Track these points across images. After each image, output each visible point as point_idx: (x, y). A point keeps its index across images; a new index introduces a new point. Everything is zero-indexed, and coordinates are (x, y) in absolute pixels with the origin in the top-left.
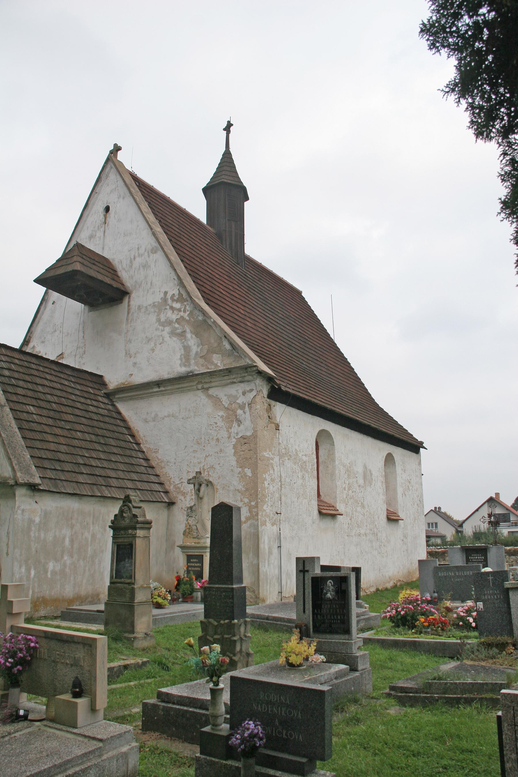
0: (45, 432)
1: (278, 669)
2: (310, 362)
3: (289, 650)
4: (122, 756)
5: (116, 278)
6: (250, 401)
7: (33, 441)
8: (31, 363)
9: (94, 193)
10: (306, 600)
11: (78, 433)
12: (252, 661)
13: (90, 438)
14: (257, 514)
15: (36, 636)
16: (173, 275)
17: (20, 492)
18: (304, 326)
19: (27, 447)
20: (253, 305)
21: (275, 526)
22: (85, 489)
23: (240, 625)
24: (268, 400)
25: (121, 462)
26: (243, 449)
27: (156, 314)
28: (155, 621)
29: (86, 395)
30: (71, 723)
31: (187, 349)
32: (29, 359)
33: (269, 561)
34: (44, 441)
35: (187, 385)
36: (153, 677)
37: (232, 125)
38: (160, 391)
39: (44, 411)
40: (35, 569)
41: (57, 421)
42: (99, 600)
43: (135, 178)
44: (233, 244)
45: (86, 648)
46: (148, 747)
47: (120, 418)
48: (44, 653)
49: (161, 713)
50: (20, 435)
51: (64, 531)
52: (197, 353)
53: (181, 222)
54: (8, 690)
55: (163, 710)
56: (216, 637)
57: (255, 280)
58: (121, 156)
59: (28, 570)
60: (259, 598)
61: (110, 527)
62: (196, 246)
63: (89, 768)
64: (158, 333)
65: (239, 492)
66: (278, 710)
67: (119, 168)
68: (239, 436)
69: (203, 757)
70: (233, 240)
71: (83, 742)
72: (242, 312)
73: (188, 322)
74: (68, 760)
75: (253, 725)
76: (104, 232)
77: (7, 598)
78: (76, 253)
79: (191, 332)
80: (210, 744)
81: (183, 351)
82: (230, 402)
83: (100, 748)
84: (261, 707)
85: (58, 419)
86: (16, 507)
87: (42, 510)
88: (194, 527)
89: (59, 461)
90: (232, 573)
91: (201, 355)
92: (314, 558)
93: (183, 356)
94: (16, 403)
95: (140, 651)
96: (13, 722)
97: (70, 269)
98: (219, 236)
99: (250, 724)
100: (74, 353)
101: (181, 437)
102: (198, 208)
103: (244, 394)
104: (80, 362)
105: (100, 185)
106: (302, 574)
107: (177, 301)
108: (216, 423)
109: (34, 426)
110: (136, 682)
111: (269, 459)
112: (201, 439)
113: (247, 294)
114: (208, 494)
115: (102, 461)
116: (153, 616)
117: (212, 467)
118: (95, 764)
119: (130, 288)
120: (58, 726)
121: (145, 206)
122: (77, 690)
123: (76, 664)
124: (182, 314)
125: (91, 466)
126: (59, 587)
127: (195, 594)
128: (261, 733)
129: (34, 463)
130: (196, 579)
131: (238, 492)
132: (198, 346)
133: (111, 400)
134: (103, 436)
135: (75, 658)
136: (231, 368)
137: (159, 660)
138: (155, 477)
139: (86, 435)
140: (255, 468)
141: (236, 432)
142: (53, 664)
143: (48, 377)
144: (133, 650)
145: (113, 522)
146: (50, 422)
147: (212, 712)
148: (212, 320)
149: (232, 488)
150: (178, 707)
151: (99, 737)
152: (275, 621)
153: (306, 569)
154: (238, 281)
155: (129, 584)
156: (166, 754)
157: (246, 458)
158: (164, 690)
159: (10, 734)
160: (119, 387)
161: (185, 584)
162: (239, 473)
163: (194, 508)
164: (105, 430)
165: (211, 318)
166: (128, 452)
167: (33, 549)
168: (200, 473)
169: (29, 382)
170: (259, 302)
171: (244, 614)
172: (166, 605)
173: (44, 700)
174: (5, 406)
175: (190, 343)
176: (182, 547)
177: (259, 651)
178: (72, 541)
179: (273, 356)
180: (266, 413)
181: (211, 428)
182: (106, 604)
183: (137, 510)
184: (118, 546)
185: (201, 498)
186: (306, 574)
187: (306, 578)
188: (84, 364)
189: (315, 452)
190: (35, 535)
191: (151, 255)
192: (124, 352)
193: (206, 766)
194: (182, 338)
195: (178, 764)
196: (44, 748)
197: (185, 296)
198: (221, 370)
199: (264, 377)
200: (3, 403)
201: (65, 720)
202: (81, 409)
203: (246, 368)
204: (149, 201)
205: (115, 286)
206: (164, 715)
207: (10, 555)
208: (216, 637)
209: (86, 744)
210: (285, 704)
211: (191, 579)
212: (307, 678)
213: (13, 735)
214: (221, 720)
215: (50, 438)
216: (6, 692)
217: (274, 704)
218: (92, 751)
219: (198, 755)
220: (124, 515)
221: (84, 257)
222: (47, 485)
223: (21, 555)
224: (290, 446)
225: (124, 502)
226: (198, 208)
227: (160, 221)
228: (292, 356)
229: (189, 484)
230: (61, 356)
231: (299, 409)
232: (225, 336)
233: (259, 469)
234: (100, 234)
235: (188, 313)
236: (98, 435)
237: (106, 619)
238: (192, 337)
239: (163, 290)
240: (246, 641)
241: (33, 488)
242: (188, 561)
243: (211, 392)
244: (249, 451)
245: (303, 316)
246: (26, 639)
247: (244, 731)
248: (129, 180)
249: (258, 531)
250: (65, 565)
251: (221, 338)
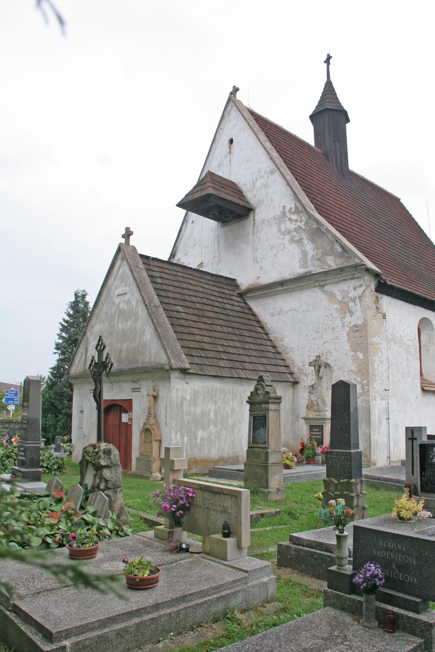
0: (192, 327)
1: (390, 521)
2: (411, 260)
3: (400, 506)
4: (263, 585)
5: (242, 198)
6: (360, 294)
7: (183, 334)
8: (178, 271)
9: (219, 129)
10: (415, 464)
11: (218, 327)
12: (367, 514)
13: (228, 330)
14: (368, 391)
15: (193, 488)
16: (290, 192)
17: (174, 375)
18: (404, 229)
19: (178, 339)
20: (358, 213)
21: (384, 400)
22: (225, 372)
23: (357, 484)
24: (376, 293)
25: (254, 350)
26: (356, 336)
27: (277, 225)
28: (285, 479)
29: (222, 296)
30: (222, 557)
31: (304, 253)
32: (176, 268)
33: (379, 431)
34: (191, 334)
35: (306, 283)
36: (284, 524)
37: (331, 57)
38: (283, 290)
39: (190, 310)
40: (187, 436)
41: (201, 317)
42: (238, 461)
43: (252, 113)
44: (339, 161)
45: (233, 498)
46: (283, 579)
47: (251, 313)
48: (199, 501)
49: (293, 552)
50: (172, 330)
51: (209, 406)
52: (313, 256)
53: (294, 147)
54: (173, 528)
55: (294, 551)
56: (336, 493)
57: (360, 191)
58: (239, 96)
59: (182, 437)
60: (370, 462)
61: (247, 402)
62: (306, 166)
63: (238, 591)
65: (353, 372)
66: (395, 556)
67: (239, 106)
68: (352, 325)
69: (330, 590)
70: (338, 157)
71: (232, 572)
72: (350, 219)
73: (304, 230)
74: (222, 584)
75: (374, 567)
76: (230, 160)
77: (169, 458)
78: (208, 179)
79: (307, 239)
80: (335, 580)
81: (301, 255)
82: (343, 296)
83: (246, 577)
84: (381, 553)
85: (202, 316)
86: (172, 387)
87: (191, 389)
88: (315, 402)
89: (204, 349)
90: (350, 440)
91: (317, 258)
92: (421, 427)
93: (301, 260)
94: (168, 304)
95: (273, 503)
96: (178, 552)
97: (204, 193)
98: (326, 155)
99: (371, 566)
100: (211, 262)
101: (303, 327)
102: (306, 133)
103: (355, 289)
104: (216, 269)
105: (224, 122)
106: (411, 441)
107: (294, 213)
108: (332, 315)
109: (183, 322)
110: (271, 528)
111: (377, 344)
112: (319, 328)
113: (353, 204)
114: (326, 374)
115: (238, 349)
116: (284, 475)
117: (329, 352)
118: (242, 589)
119: (255, 205)
120: (212, 558)
121: (262, 136)
122: (227, 531)
123: (224, 511)
124: (299, 224)
125: (229, 353)
126: (206, 450)
127: (316, 458)
128: (381, 574)
129: (184, 352)
130: (318, 445)
131: (351, 373)
132: (314, 250)
133: (243, 299)
134: (238, 329)
135: (224, 506)
136: (343, 268)
137: (289, 510)
138: (282, 361)
139: (224, 328)
140: (366, 352)
141: (349, 322)
142: (207, 510)
143: (192, 282)
144: (267, 501)
145: (249, 398)
146: (195, 318)
147: (337, 554)
148: (325, 227)
149: (346, 369)
150: (307, 549)
151: (245, 569)
152: (386, 481)
153: (414, 437)
154: (344, 193)
155: (264, 448)
156: (298, 586)
158: (295, 535)
159: (176, 561)
160: (249, 287)
161: (308, 449)
162: (353, 356)
163: (315, 386)
164: (240, 323)
165: (323, 225)
166: (259, 341)
167: (186, 421)
168: (319, 357)
169: (177, 287)
170: (363, 210)
171: (360, 474)
172: (293, 466)
173: (199, 537)
174: (159, 307)
175: (306, 248)
176: (305, 419)
177: (372, 506)
178: (216, 414)
179: (378, 256)
180: (374, 304)
181: (328, 319)
182: (245, 464)
183: (269, 387)
184: (255, 418)
185: (321, 378)
186: (415, 441)
187: (414, 445)
188: (220, 270)
189: (417, 337)
190: (187, 409)
191: (270, 177)
192: (252, 259)
193: (332, 598)
194: (300, 244)
195: (307, 594)
196: (202, 574)
197: (300, 208)
198: (334, 270)
199: (371, 273)
200: (157, 305)
201: (218, 555)
202: (219, 307)
203: (356, 267)
204: (265, 131)
205: (242, 204)
206: (295, 555)
207: (168, 426)
208: (336, 493)
209: (234, 573)
210: (401, 551)
211: (313, 445)
212: (416, 530)
213: (179, 562)
214: (345, 562)
215: (196, 331)
216: (172, 530)
217: (392, 551)
218: (239, 579)
219: (326, 588)
220: (259, 392)
221: (215, 182)
222: (195, 369)
223: (176, 425)
224: (395, 332)
225: (258, 381)
226: (306, 133)
227: (275, 147)
228: (394, 254)
229: (310, 366)
230: (201, 265)
231: (402, 300)
232: (336, 241)
233: (369, 352)
234: (226, 162)
235: (304, 222)
236: (234, 328)
237: (246, 477)
238: (308, 243)
239: (282, 205)
240: (362, 497)
241: (184, 372)
242: (311, 430)
243: (326, 288)
244: (360, 337)
245: (403, 220)
246: (185, 490)
247: (366, 572)
248: (248, 115)
249: (369, 405)
250: (211, 433)
251: (333, 242)
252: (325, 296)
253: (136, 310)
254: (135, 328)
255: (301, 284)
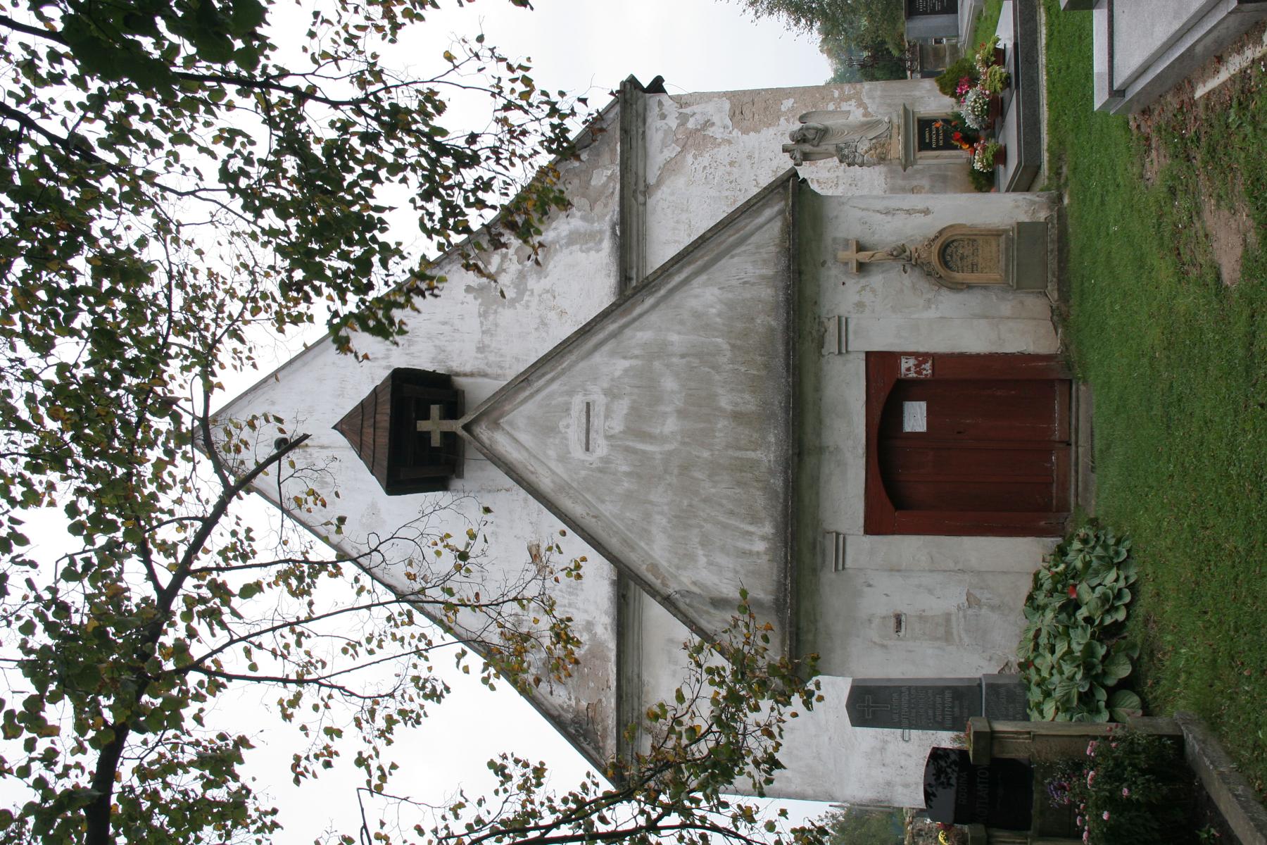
35: (634, 219)
52: (583, 218)
64: (535, 300)
91: (588, 208)
157: (766, 109)
162: (788, 120)
243: (652, 180)
252: (668, 182)
253: (636, 357)
254: (683, 356)
255: (634, 232)
